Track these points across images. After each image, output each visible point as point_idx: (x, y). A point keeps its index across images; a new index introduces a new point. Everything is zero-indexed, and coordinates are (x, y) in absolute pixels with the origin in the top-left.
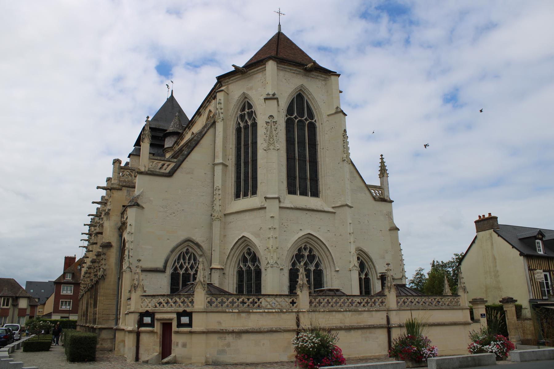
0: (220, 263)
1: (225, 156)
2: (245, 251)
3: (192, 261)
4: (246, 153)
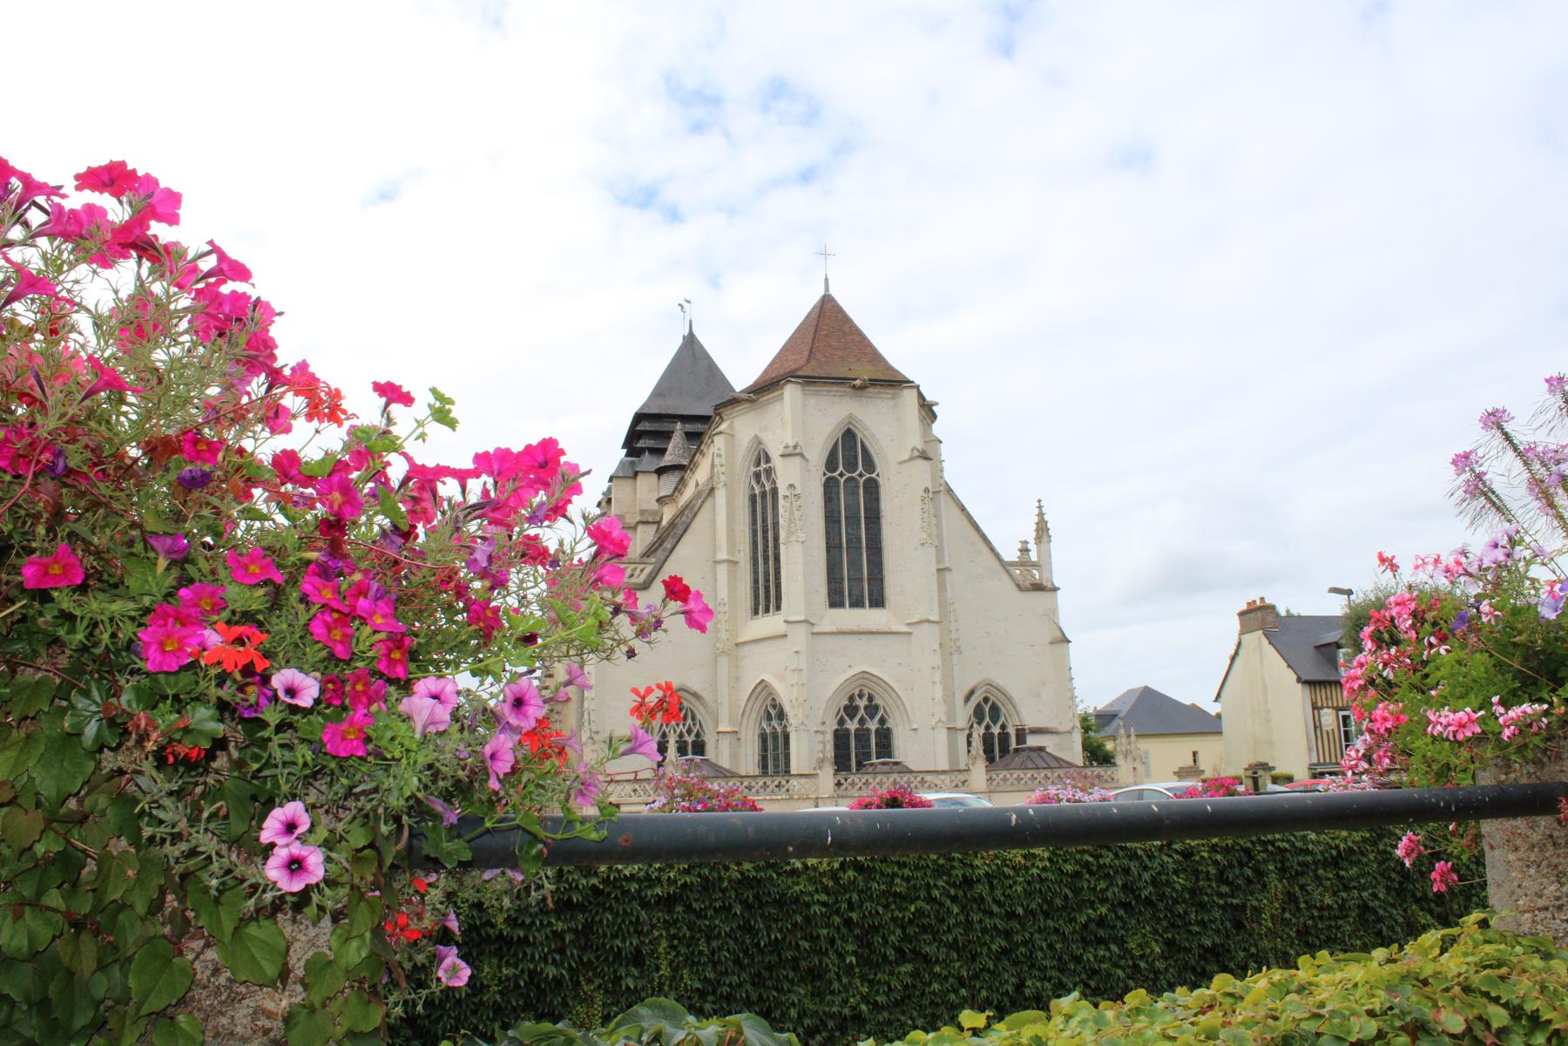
0: (731, 721)
1: (732, 544)
2: (769, 702)
3: (689, 721)
4: (765, 539)
